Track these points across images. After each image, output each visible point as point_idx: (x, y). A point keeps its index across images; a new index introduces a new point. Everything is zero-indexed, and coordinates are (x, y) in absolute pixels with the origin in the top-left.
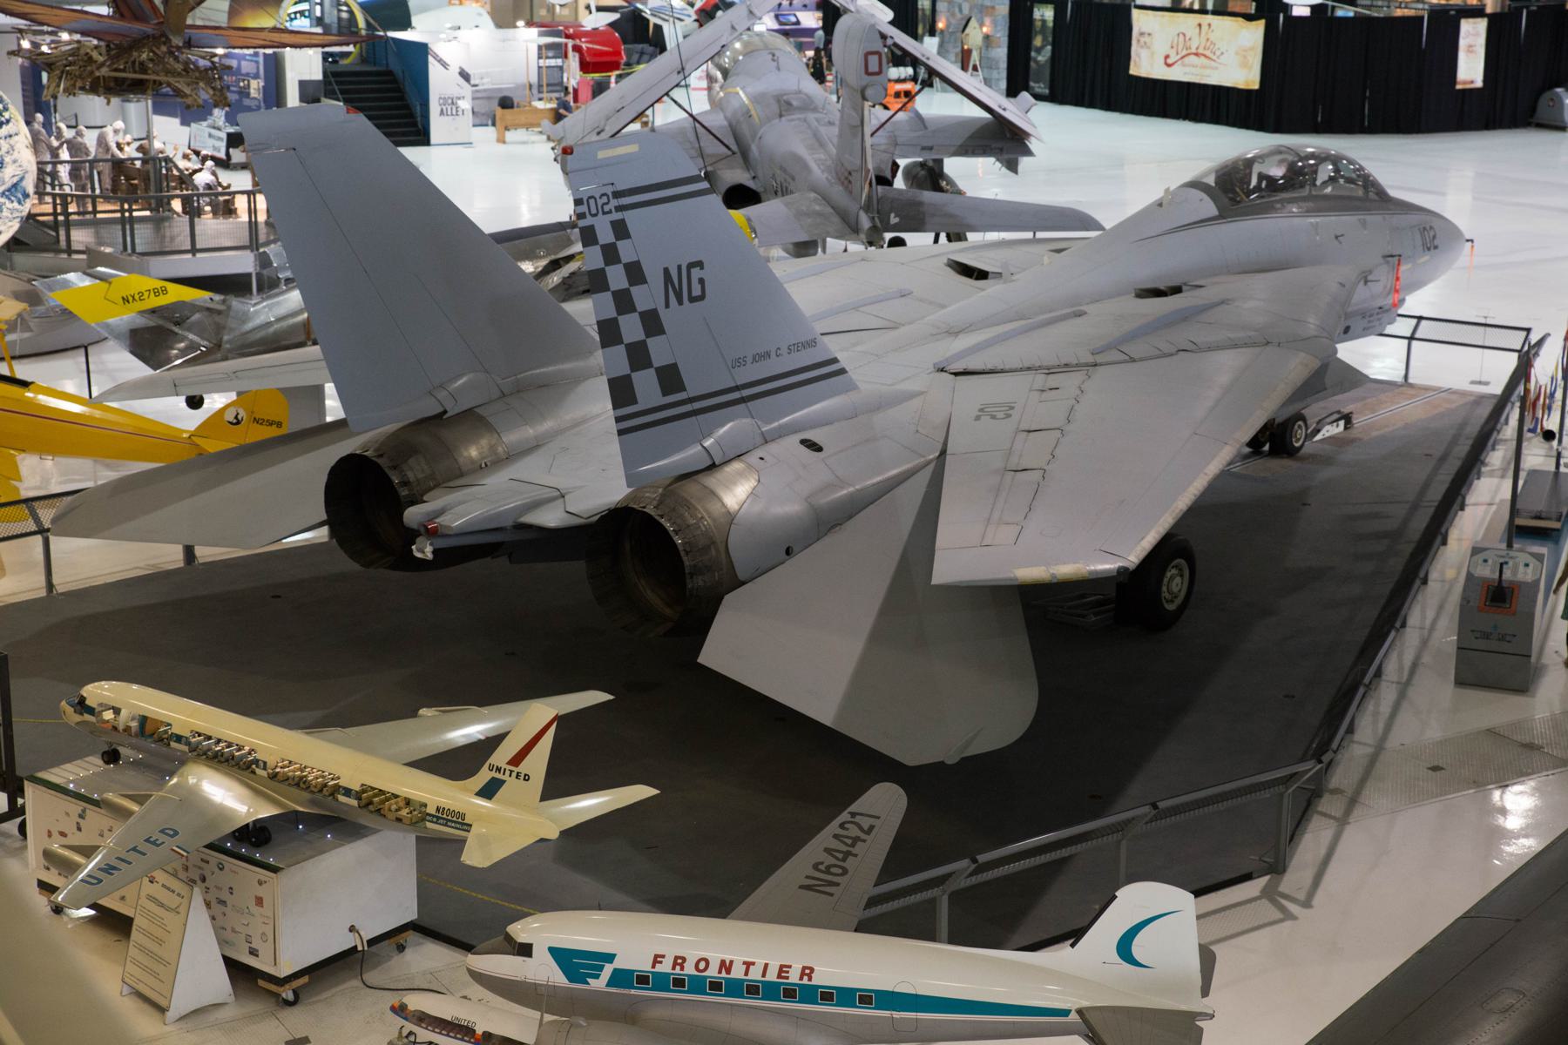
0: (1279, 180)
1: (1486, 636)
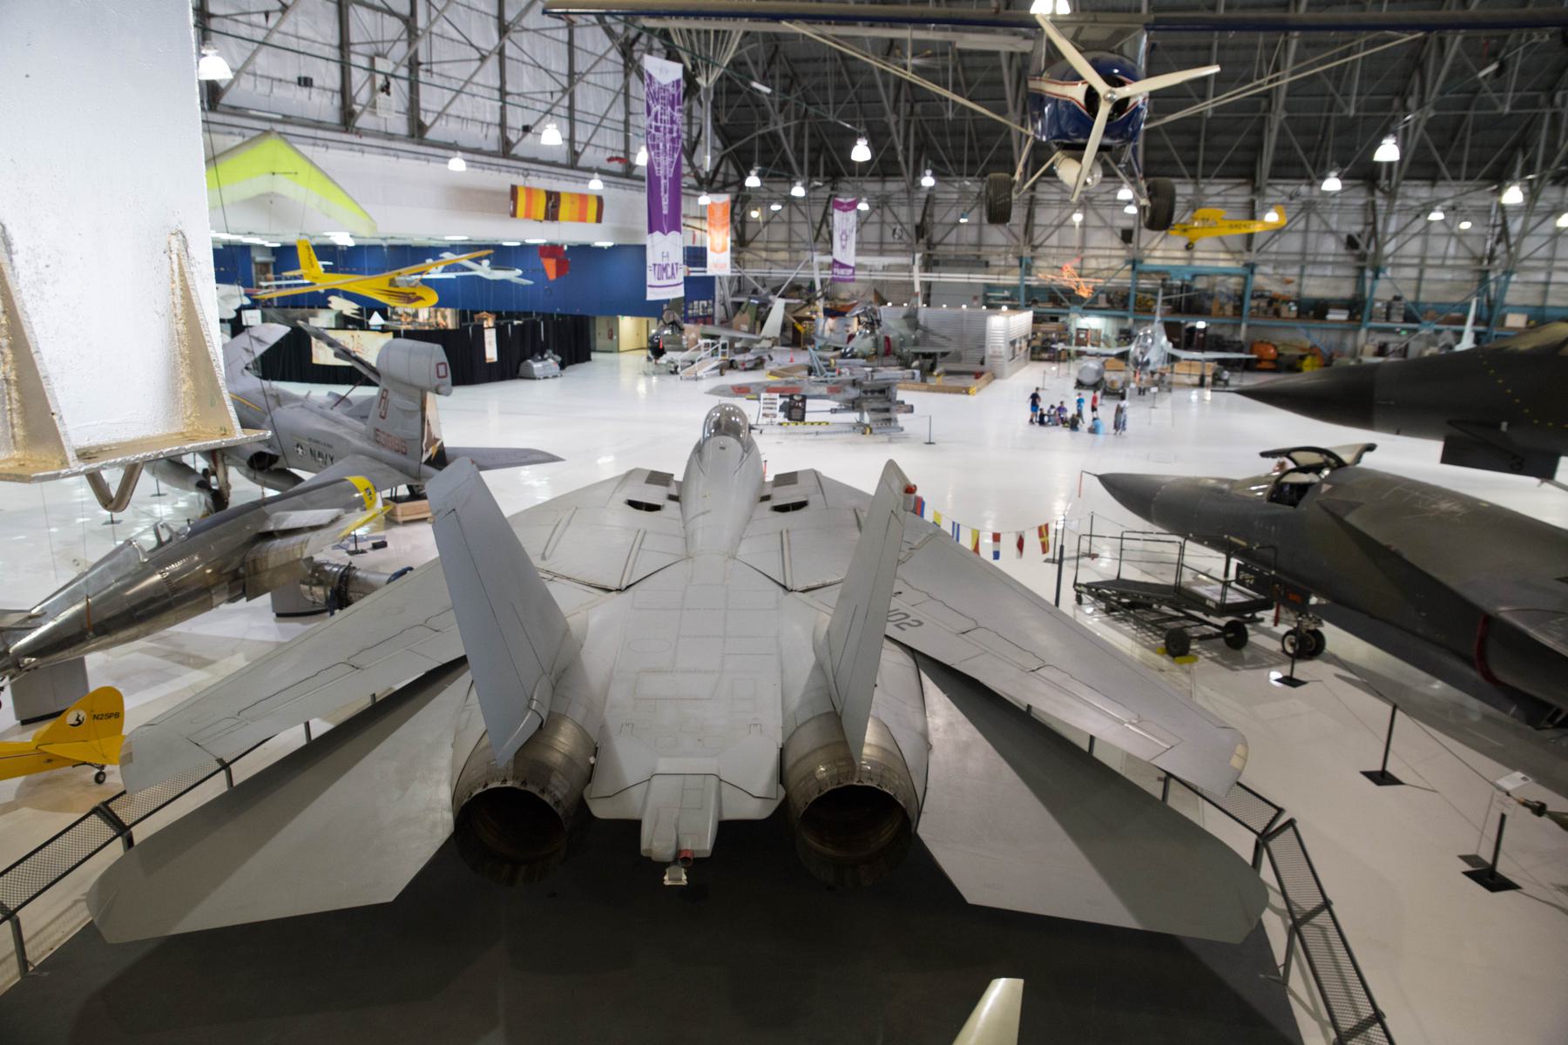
0: (742, 208)
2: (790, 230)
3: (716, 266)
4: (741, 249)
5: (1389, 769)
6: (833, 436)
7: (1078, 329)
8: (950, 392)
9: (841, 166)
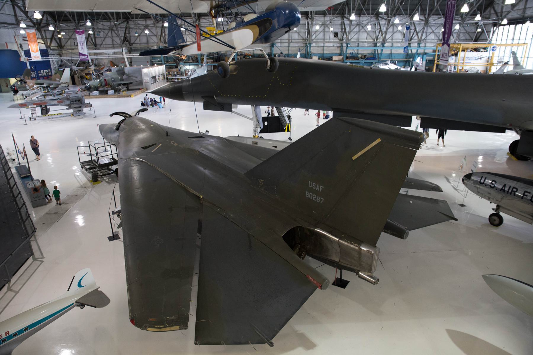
1: (36, 197)
2: (113, 40)
3: (35, 57)
4: (61, 49)
6: (60, 119)
7: (185, 70)
8: (125, 97)
9: (128, 15)
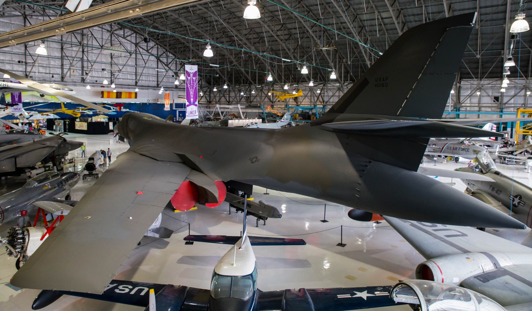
5: (325, 219)
